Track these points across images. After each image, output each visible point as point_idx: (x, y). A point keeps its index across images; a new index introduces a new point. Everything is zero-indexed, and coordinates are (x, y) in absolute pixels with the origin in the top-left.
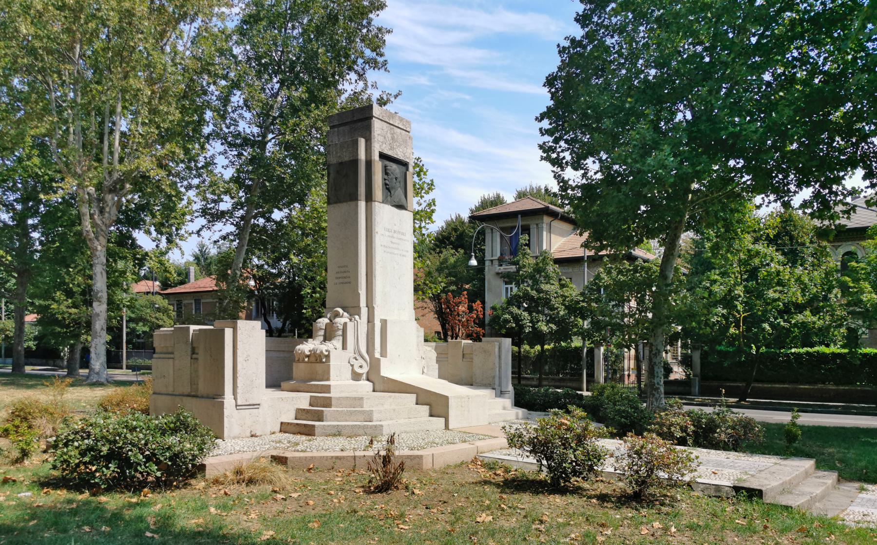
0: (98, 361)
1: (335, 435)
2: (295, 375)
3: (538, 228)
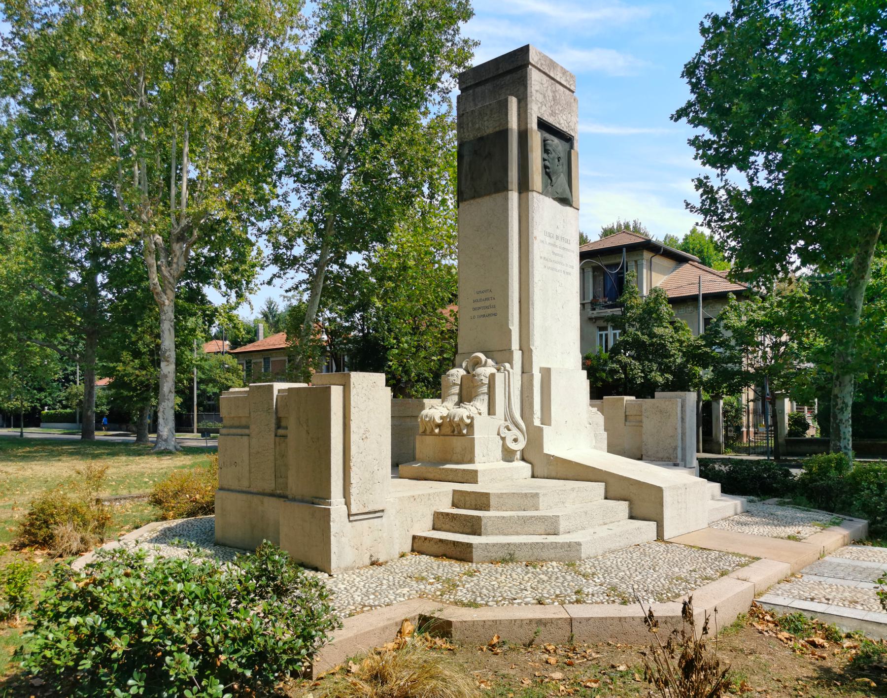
0: (166, 426)
1: (504, 561)
2: (418, 454)
3: (637, 265)
